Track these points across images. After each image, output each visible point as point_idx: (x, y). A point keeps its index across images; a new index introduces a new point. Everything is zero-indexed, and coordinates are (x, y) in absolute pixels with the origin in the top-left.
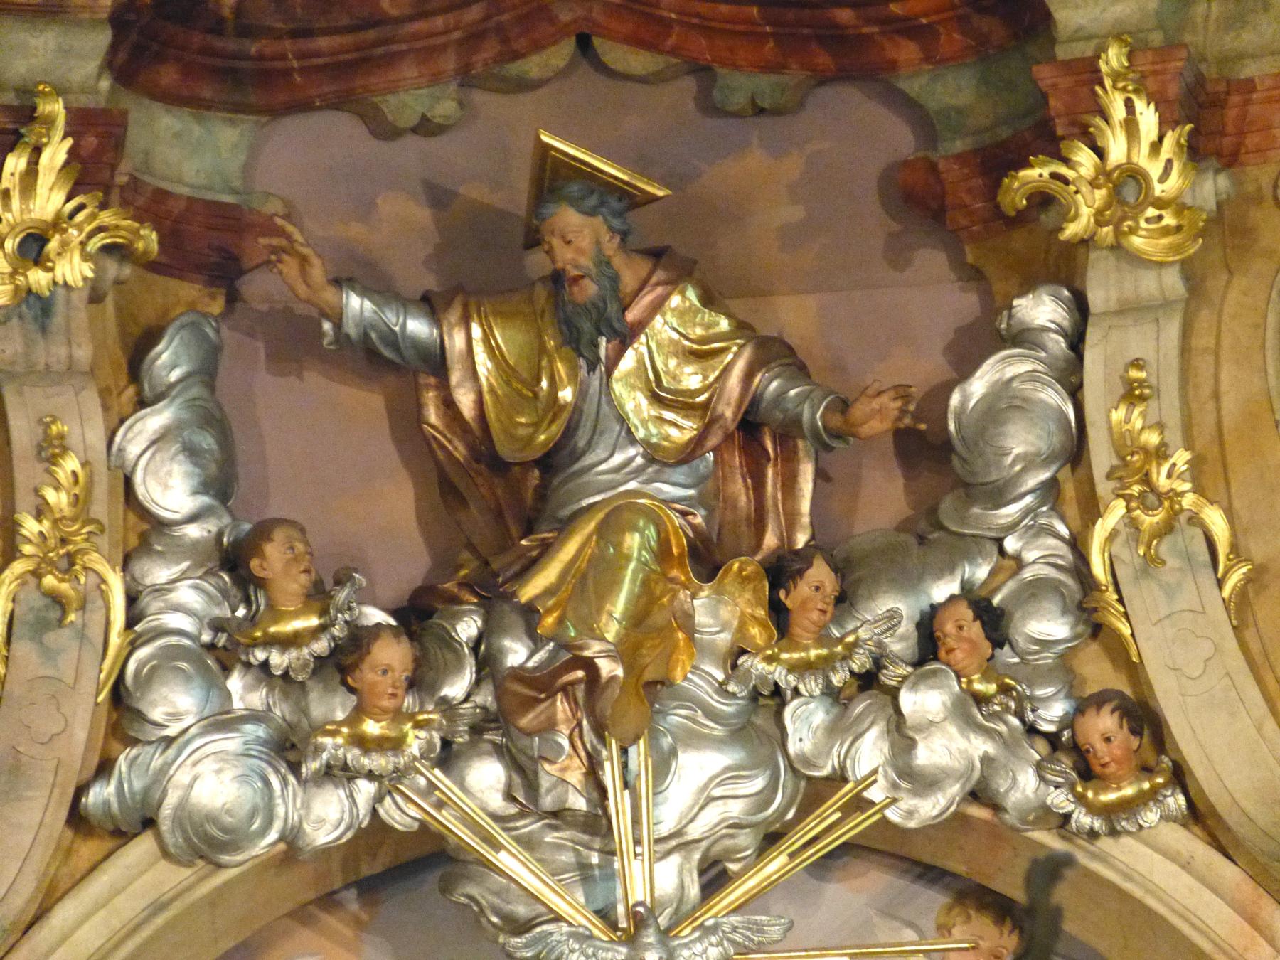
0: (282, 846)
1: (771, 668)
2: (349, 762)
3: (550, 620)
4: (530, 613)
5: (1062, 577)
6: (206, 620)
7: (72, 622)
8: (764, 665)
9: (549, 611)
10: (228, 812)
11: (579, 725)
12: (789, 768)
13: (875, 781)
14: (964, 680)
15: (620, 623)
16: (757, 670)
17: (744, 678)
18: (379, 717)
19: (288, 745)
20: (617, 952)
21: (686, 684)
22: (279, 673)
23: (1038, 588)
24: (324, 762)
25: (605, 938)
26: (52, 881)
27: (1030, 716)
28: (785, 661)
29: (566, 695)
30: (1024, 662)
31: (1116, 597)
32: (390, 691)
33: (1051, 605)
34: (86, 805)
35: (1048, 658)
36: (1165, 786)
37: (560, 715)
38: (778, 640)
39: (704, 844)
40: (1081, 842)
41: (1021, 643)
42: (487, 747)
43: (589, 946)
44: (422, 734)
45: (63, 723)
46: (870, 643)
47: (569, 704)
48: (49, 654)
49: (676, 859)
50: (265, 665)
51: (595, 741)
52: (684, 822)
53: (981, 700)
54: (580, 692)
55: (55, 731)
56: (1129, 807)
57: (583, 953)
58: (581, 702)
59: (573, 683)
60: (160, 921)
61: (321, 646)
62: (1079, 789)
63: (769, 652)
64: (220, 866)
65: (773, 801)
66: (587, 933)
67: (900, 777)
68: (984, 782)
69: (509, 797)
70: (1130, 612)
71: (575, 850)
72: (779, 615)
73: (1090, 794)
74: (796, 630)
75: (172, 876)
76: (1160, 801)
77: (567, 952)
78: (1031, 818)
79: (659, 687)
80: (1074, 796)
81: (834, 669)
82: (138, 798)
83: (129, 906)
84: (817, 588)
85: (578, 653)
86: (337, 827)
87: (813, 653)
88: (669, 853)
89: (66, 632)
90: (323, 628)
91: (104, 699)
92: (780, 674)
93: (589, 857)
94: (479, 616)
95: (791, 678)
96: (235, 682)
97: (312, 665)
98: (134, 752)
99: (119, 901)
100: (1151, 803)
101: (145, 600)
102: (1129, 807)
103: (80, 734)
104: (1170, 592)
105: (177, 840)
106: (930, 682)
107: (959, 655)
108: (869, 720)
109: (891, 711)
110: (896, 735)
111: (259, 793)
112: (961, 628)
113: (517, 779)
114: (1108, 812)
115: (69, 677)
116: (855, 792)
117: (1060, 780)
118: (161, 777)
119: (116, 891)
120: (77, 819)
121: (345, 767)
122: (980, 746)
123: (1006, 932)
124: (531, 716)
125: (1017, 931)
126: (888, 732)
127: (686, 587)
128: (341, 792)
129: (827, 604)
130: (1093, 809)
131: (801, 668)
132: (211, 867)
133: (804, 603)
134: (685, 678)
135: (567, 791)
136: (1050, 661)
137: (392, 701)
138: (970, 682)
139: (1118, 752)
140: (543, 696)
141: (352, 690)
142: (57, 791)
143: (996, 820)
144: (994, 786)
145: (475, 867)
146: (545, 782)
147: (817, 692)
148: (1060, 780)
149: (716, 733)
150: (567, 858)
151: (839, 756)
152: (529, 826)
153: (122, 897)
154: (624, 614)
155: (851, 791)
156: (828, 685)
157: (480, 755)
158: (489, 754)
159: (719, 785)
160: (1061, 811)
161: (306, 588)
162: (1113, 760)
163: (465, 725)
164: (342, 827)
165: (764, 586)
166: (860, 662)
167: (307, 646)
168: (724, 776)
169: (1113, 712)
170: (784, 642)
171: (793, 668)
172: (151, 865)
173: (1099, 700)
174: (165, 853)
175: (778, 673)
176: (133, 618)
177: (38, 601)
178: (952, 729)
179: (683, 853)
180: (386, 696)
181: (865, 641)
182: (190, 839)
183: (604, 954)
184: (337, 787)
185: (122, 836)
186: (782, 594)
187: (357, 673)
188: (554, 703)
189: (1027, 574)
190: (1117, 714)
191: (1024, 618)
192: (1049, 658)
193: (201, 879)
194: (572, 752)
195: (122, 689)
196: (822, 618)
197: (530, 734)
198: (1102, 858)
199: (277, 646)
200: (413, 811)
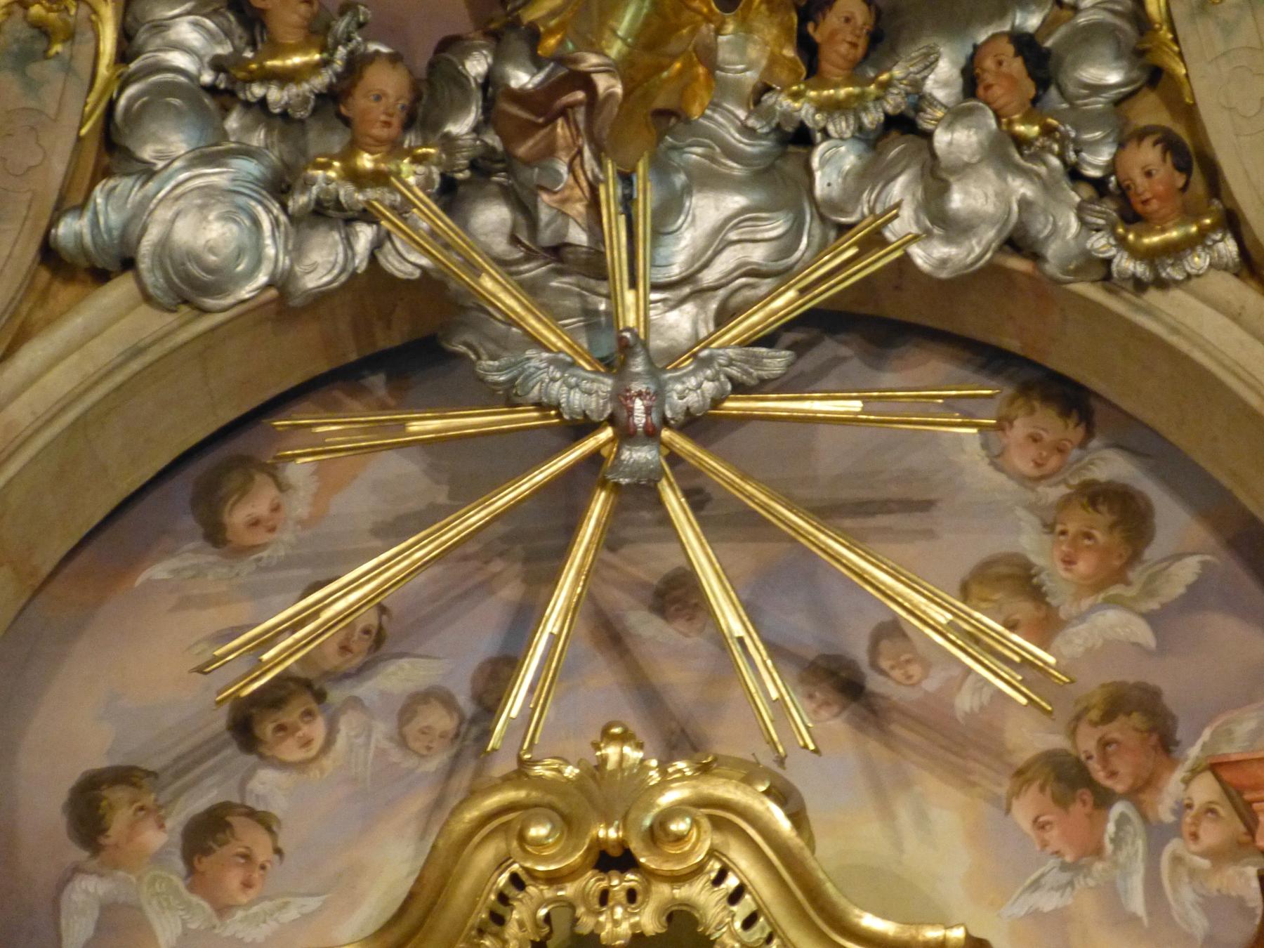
0: (273, 293)
1: (797, 105)
2: (342, 199)
3: (552, 42)
4: (534, 36)
5: (1118, 21)
6: (207, 59)
7: (57, 53)
8: (789, 101)
9: (551, 32)
10: (212, 250)
11: (580, 152)
12: (816, 215)
13: (896, 216)
14: (1004, 120)
15: (624, 40)
16: (781, 107)
17: (768, 114)
18: (373, 149)
19: (283, 186)
20: (603, 383)
21: (706, 122)
22: (277, 111)
23: (1092, 32)
24: (313, 196)
25: (588, 368)
26: (23, 322)
27: (1072, 156)
28: (811, 100)
29: (567, 120)
30: (1073, 106)
31: (1170, 36)
32: (383, 118)
33: (1106, 50)
34: (56, 235)
35: (1098, 103)
36: (1213, 228)
37: (561, 142)
38: (808, 77)
39: (722, 293)
40: (1127, 295)
41: (1071, 89)
42: (495, 189)
43: (574, 376)
44: (420, 169)
45: (40, 157)
46: (905, 82)
47: (570, 131)
48: (31, 86)
49: (689, 308)
50: (263, 102)
51: (597, 170)
52: (697, 266)
53: (1021, 142)
54: (580, 116)
55: (33, 163)
56: (1176, 251)
57: (565, 383)
58: (582, 126)
59: (572, 106)
60: (135, 366)
61: (321, 81)
62: (1120, 230)
63: (795, 88)
64: (205, 311)
65: (796, 249)
66: (568, 359)
67: (932, 223)
68: (1021, 226)
69: (514, 240)
70: (1184, 51)
71: (580, 295)
72: (809, 51)
73: (1131, 237)
74: (826, 66)
75: (153, 322)
76: (1210, 247)
77: (547, 380)
78: (1072, 267)
79: (673, 120)
80: (1116, 239)
81: (866, 109)
82: (116, 233)
83: (105, 350)
84: (847, 20)
85: (573, 67)
86: (330, 272)
87: (843, 92)
88: (683, 301)
89: (52, 63)
90: (325, 63)
91: (91, 131)
92: (807, 112)
93: (596, 304)
94: (490, 51)
95: (818, 117)
96: (233, 122)
97: (312, 104)
98: (111, 183)
99: (94, 345)
100: (1199, 248)
101: (142, 36)
102: (1176, 251)
103: (59, 167)
104: (1228, 29)
105: (157, 280)
106: (967, 121)
107: (997, 91)
108: (904, 163)
109: (926, 155)
110: (930, 180)
111: (246, 231)
112: (1000, 63)
113: (521, 220)
114: (1151, 256)
115: (51, 110)
116: (874, 225)
117: (1101, 222)
118: (139, 217)
119: (91, 335)
120: (49, 254)
121: (338, 205)
122: (1022, 188)
123: (1071, 425)
124: (530, 143)
125: (1083, 425)
126: (922, 176)
127: (708, 20)
128: (336, 236)
129: (858, 37)
130: (1136, 253)
131: (831, 108)
132: (196, 312)
133: (833, 34)
134: (703, 116)
135: (567, 225)
136: (1100, 106)
137: (386, 130)
138: (1010, 123)
139: (1160, 188)
140: (541, 120)
141: (347, 122)
142: (28, 224)
143: (1037, 273)
144: (1033, 232)
145: (475, 314)
146: (544, 215)
147: (848, 134)
148: (1101, 222)
149: (736, 173)
150: (571, 303)
151: (869, 202)
152: (532, 270)
153: (97, 341)
154: (629, 33)
155: (869, 225)
156: (861, 127)
157: (487, 197)
158: (495, 196)
159: (735, 227)
160: (1101, 256)
161: (305, 19)
162: (1154, 197)
163: (466, 158)
164: (336, 271)
165: (791, 19)
166: (893, 104)
167: (307, 81)
168: (742, 218)
169: (1155, 143)
170: (812, 81)
171: (822, 106)
172: (131, 309)
173: (1141, 135)
174: (148, 298)
175: (805, 111)
176: (124, 54)
177: (26, 33)
178: (990, 173)
179: (699, 301)
180: (378, 124)
181: (900, 80)
182: (172, 279)
183: (588, 385)
184: (332, 229)
185: (101, 276)
186: (810, 27)
187: (350, 100)
188: (554, 129)
189: (1082, 20)
190: (1159, 147)
191: (1076, 64)
192: (1100, 103)
193: (182, 326)
194: (571, 181)
195: (112, 128)
196: (853, 51)
197: (528, 163)
198: (1149, 311)
199: (275, 82)
200: (416, 258)
